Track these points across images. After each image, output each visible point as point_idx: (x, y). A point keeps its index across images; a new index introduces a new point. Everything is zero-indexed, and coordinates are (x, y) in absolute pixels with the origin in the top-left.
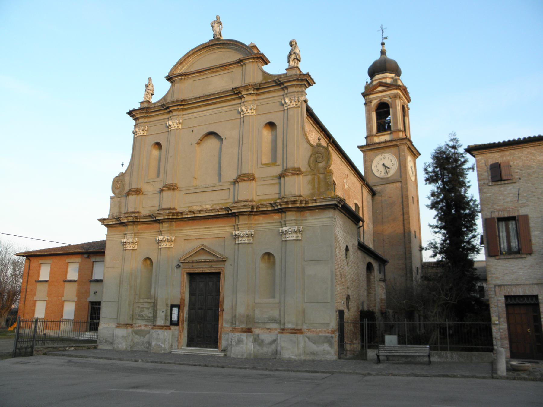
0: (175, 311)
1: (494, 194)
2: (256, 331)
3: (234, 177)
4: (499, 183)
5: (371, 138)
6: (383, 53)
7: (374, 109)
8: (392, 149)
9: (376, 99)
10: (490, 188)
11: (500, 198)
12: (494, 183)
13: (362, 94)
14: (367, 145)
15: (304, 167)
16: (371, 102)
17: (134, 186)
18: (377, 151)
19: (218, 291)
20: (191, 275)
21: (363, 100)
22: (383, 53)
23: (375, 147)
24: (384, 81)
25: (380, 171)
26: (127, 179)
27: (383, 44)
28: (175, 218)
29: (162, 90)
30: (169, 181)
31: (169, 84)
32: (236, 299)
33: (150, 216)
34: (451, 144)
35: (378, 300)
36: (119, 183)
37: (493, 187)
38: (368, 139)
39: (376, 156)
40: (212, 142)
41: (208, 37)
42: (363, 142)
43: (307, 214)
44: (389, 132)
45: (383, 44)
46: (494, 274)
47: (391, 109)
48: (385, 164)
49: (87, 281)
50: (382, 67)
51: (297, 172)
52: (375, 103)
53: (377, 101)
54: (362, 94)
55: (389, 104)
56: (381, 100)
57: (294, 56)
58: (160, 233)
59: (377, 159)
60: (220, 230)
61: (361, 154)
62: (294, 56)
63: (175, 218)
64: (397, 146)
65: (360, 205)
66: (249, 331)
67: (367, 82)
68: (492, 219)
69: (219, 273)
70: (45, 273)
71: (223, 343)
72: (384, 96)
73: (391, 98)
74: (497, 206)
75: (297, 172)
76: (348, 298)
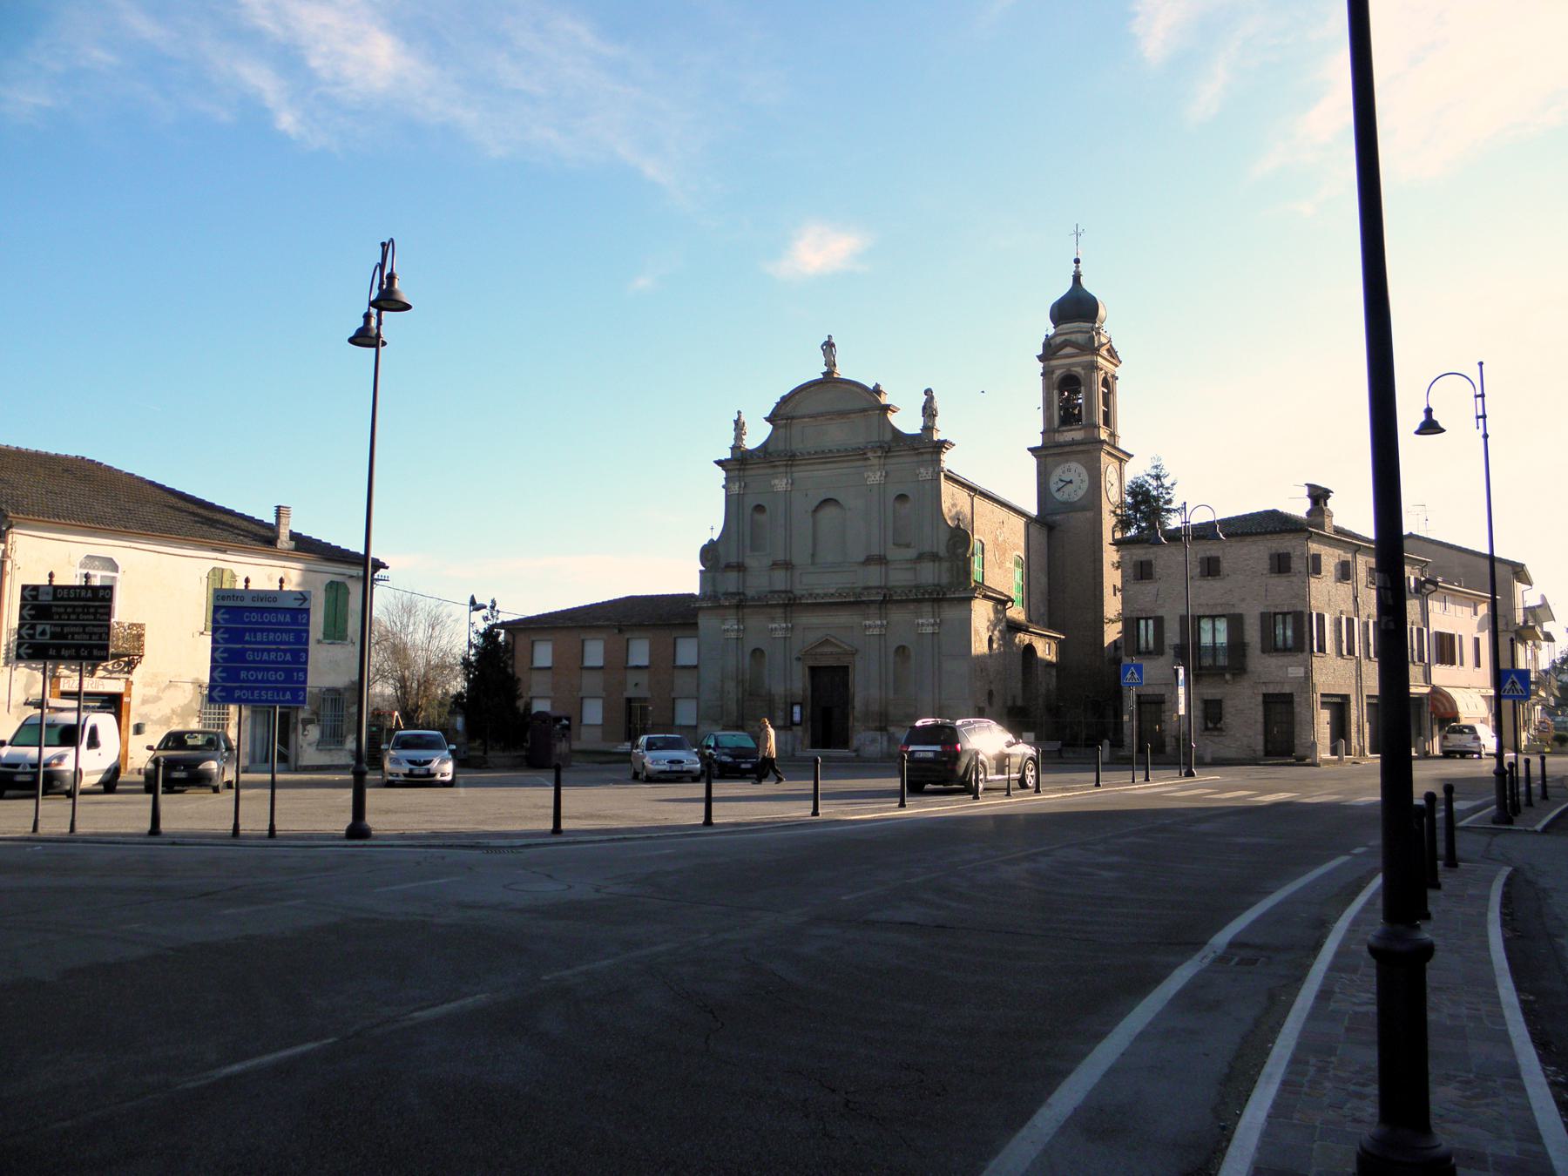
0: (797, 709)
2: (892, 729)
3: (862, 559)
6: (1077, 278)
14: (1043, 447)
15: (943, 552)
17: (733, 560)
19: (846, 685)
20: (814, 671)
21: (1039, 367)
22: (1077, 278)
24: (1073, 337)
26: (721, 550)
27: (1077, 261)
28: (791, 604)
29: (757, 435)
30: (780, 557)
31: (769, 427)
32: (865, 690)
33: (759, 599)
34: (1153, 472)
35: (1042, 690)
36: (709, 553)
39: (1058, 464)
40: (829, 512)
41: (816, 371)
42: (1038, 442)
43: (945, 605)
45: (1077, 261)
49: (664, 664)
50: (1077, 309)
51: (934, 557)
52: (1058, 373)
57: (929, 411)
58: (773, 620)
59: (1081, 493)
60: (843, 618)
62: (929, 411)
63: (791, 604)
64: (1087, 452)
66: (882, 729)
69: (845, 669)
70: (595, 653)
71: (855, 743)
72: (1073, 365)
75: (934, 557)
76: (990, 694)
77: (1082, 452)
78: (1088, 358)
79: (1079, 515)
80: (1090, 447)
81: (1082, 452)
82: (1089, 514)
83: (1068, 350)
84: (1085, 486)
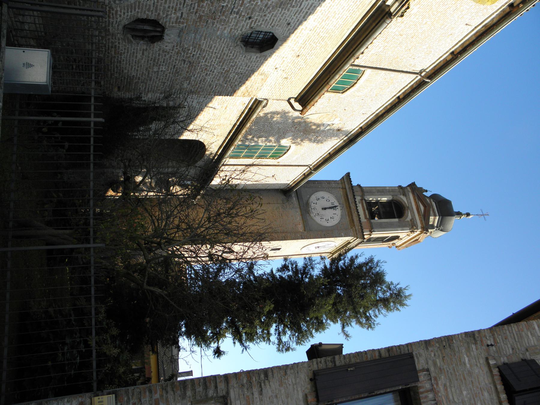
1: (470, 373)
4: (500, 387)
5: (360, 193)
6: (459, 214)
7: (395, 198)
8: (347, 220)
9: (410, 201)
10: (482, 361)
11: (465, 393)
12: (496, 371)
13: (413, 184)
16: (404, 194)
18: (343, 200)
22: (459, 214)
23: (349, 197)
25: (318, 202)
37: (486, 369)
38: (359, 189)
44: (368, 217)
46: (261, 393)
47: (397, 220)
48: (325, 208)
52: (404, 199)
53: (406, 202)
54: (413, 184)
55: (403, 218)
56: (408, 207)
59: (317, 219)
61: (337, 176)
65: (282, 160)
67: (426, 191)
68: (414, 374)
73: (411, 220)
74: (445, 385)
77: (352, 221)
78: (419, 225)
79: (299, 218)
80: (358, 227)
81: (352, 221)
82: (300, 228)
83: (422, 208)
84: (324, 223)
